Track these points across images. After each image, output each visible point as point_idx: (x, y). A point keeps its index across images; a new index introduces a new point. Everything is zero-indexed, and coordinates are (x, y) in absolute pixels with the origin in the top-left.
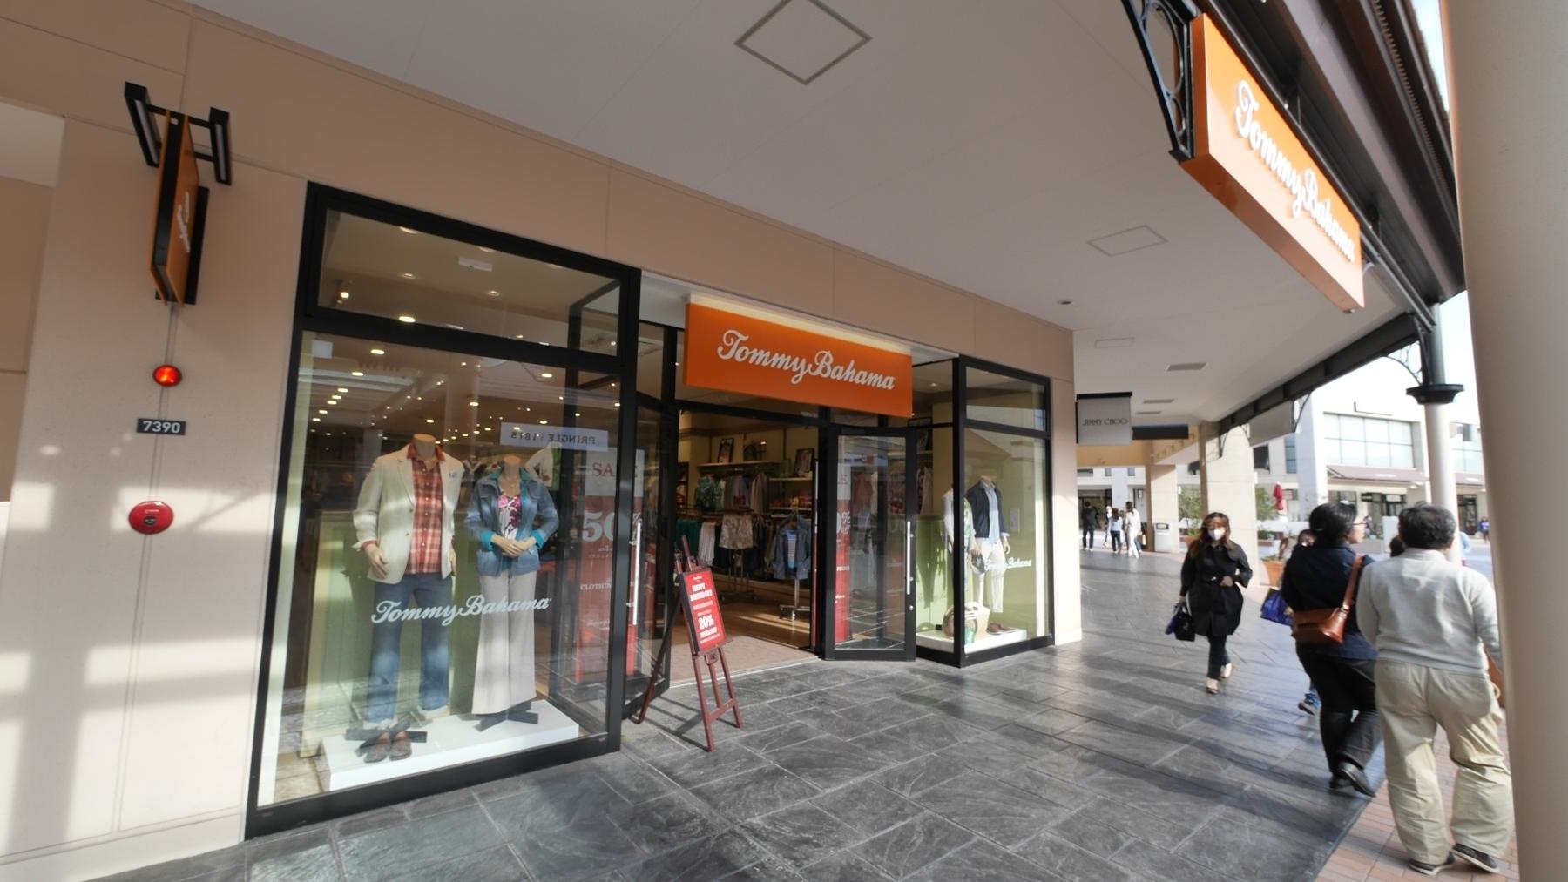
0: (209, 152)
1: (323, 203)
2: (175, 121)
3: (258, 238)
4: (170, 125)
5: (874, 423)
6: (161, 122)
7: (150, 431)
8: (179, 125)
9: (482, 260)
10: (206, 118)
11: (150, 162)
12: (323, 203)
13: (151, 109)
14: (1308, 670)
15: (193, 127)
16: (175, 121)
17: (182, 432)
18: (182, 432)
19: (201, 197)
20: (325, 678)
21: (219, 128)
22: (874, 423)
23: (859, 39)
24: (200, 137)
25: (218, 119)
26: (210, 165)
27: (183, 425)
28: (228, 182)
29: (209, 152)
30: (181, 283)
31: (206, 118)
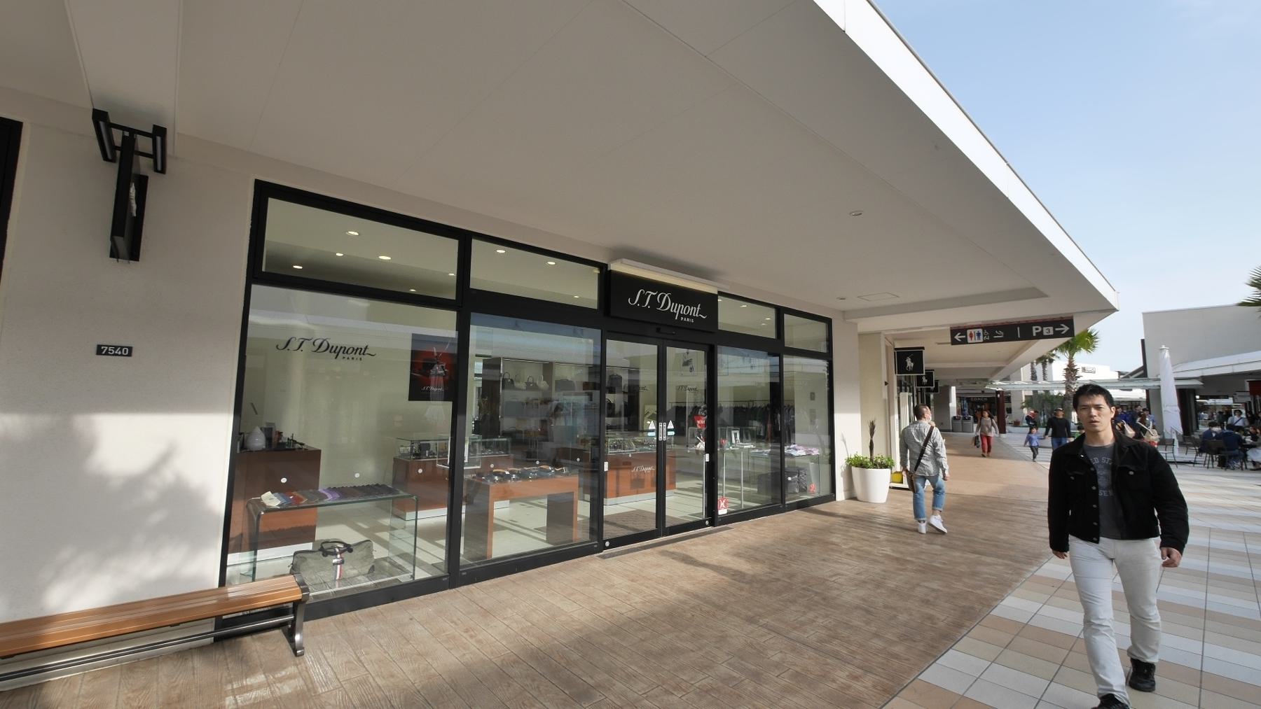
0: (150, 151)
1: (264, 192)
2: (127, 134)
3: (200, 227)
4: (124, 137)
5: (583, 290)
6: (118, 137)
7: (107, 354)
8: (132, 134)
9: (354, 229)
10: (150, 131)
11: (105, 158)
12: (264, 192)
13: (110, 126)
14: (1050, 528)
15: (139, 137)
16: (127, 134)
17: (130, 355)
18: (130, 355)
19: (142, 183)
20: (233, 552)
21: (159, 139)
22: (583, 290)
23: (788, 318)
24: (144, 144)
25: (159, 132)
26: (151, 161)
27: (130, 349)
28: (163, 171)
29: (150, 151)
30: (127, 236)
31: (150, 131)
